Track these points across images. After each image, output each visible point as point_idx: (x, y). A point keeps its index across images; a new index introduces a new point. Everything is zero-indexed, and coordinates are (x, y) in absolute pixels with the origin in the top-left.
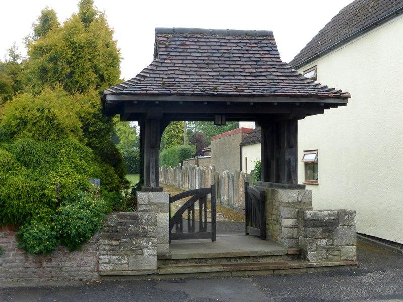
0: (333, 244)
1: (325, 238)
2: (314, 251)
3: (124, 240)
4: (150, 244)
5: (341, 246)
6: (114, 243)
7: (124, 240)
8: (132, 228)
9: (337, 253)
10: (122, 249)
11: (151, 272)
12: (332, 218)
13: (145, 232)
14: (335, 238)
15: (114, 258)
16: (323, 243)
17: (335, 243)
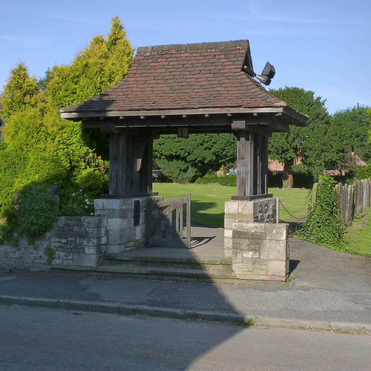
0: (259, 258)
1: (251, 250)
2: (240, 263)
3: (70, 239)
4: (91, 244)
5: (269, 260)
6: (63, 241)
7: (70, 239)
8: (76, 229)
9: (264, 267)
10: (68, 247)
11: (90, 269)
12: (259, 230)
13: (87, 232)
14: (262, 251)
15: (62, 254)
16: (249, 256)
17: (262, 257)
